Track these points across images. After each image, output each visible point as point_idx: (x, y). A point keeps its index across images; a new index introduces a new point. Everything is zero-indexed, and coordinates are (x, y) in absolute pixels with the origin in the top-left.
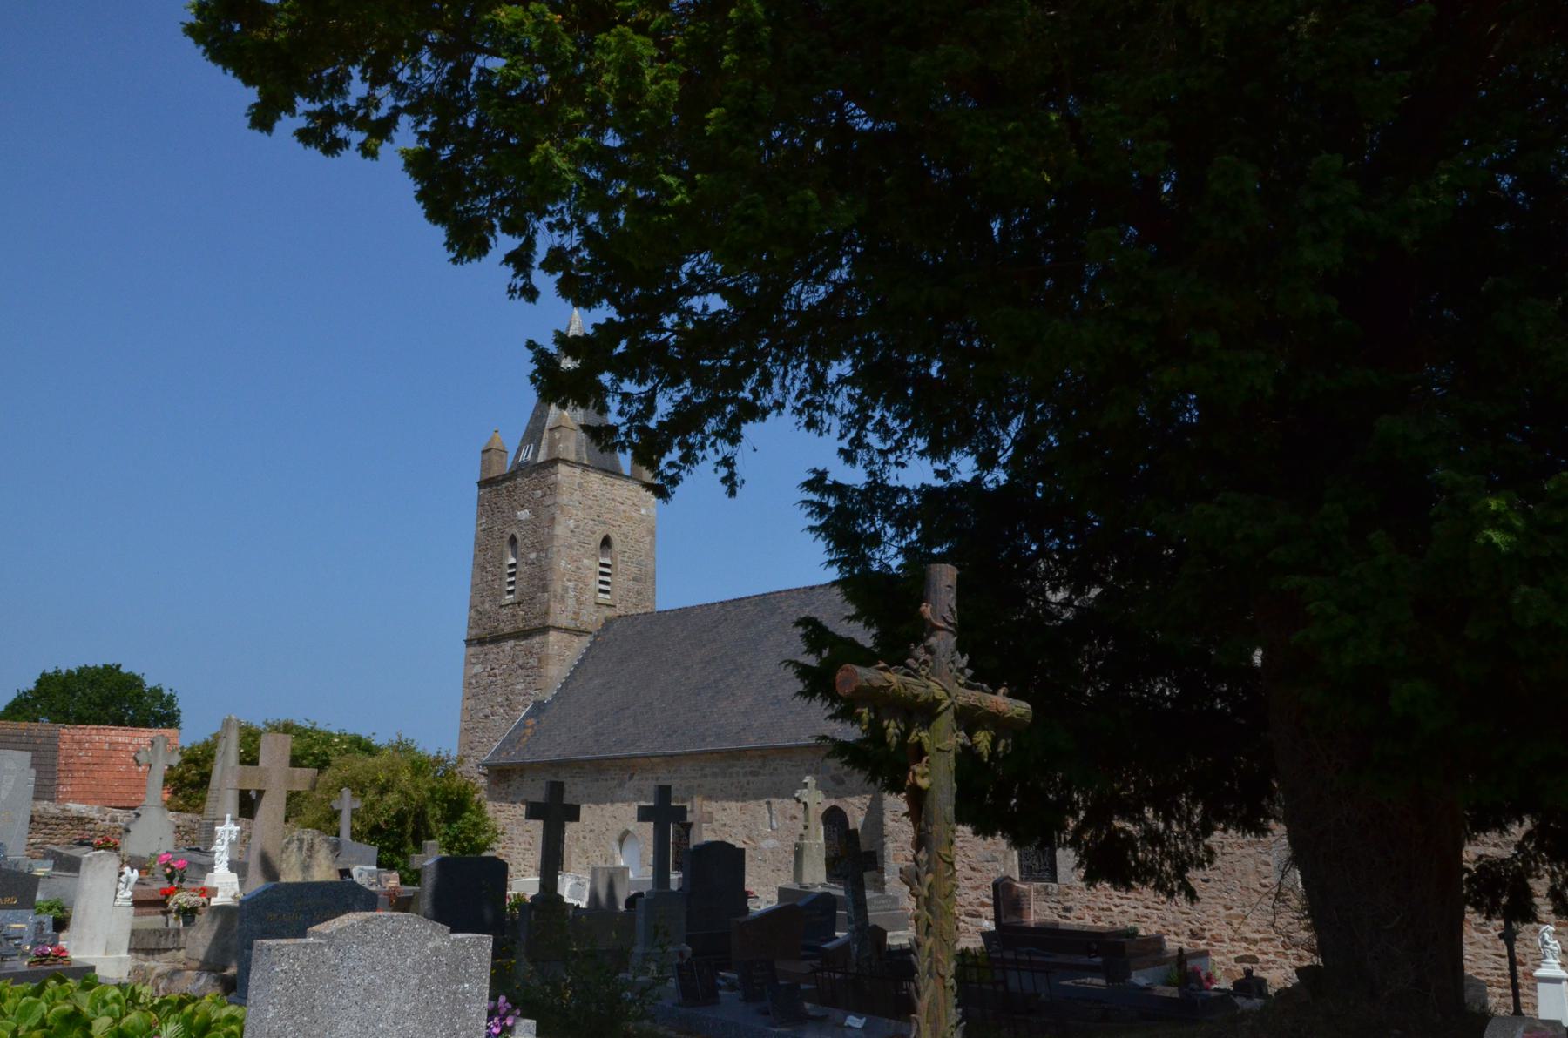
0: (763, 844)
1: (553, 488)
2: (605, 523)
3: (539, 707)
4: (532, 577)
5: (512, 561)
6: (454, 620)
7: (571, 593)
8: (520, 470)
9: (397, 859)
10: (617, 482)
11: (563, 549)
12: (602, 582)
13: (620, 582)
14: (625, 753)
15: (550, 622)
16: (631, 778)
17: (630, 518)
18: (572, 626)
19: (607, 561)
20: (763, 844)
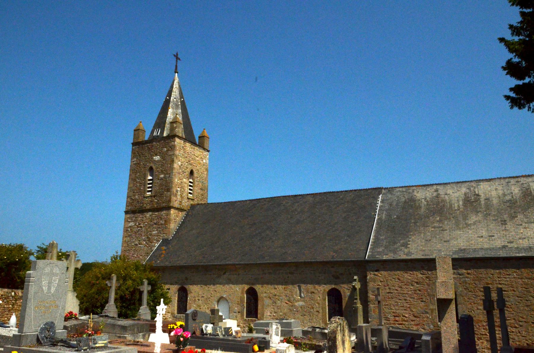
0: (296, 304)
1: (173, 148)
2: (191, 164)
3: (166, 242)
4: (161, 185)
5: (150, 178)
6: (121, 203)
7: (179, 193)
8: (153, 139)
9: (129, 312)
10: (196, 148)
11: (177, 174)
12: (190, 189)
13: (196, 189)
14: (223, 263)
15: (171, 204)
16: (224, 274)
17: (200, 163)
18: (179, 207)
19: (191, 180)
20: (296, 304)
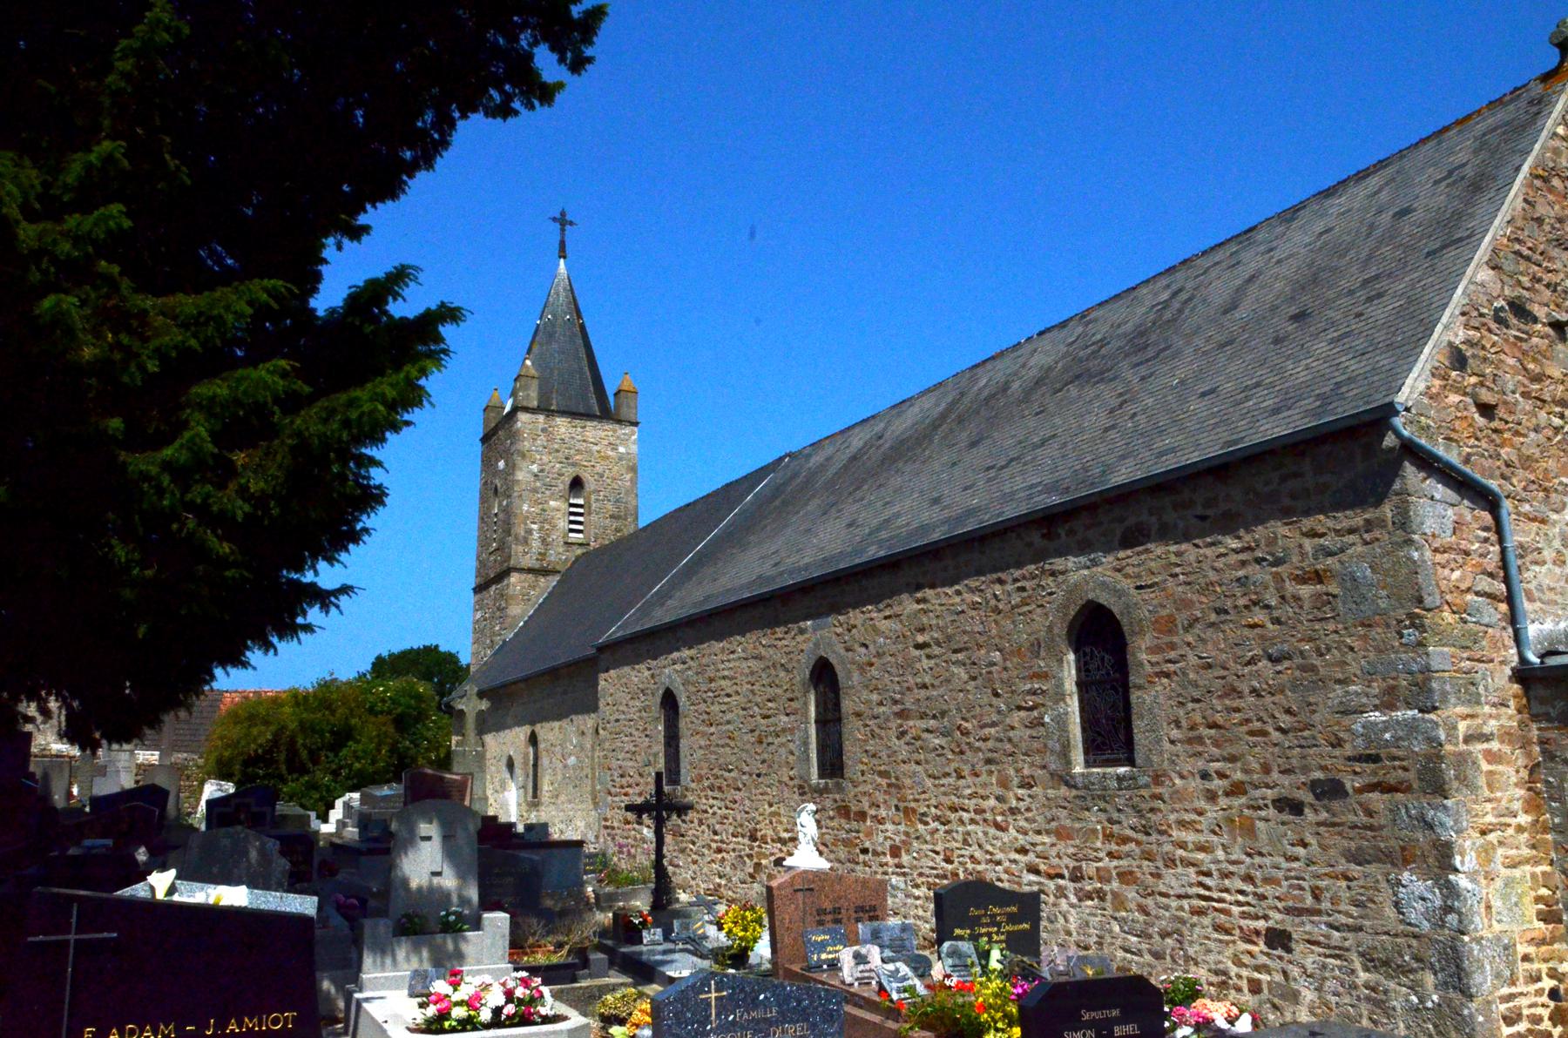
2: (574, 465)
7: (536, 535)
15: (512, 563)
